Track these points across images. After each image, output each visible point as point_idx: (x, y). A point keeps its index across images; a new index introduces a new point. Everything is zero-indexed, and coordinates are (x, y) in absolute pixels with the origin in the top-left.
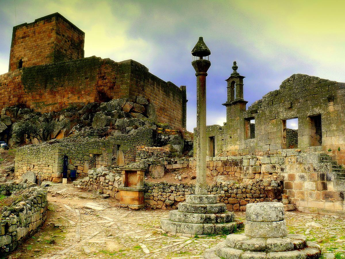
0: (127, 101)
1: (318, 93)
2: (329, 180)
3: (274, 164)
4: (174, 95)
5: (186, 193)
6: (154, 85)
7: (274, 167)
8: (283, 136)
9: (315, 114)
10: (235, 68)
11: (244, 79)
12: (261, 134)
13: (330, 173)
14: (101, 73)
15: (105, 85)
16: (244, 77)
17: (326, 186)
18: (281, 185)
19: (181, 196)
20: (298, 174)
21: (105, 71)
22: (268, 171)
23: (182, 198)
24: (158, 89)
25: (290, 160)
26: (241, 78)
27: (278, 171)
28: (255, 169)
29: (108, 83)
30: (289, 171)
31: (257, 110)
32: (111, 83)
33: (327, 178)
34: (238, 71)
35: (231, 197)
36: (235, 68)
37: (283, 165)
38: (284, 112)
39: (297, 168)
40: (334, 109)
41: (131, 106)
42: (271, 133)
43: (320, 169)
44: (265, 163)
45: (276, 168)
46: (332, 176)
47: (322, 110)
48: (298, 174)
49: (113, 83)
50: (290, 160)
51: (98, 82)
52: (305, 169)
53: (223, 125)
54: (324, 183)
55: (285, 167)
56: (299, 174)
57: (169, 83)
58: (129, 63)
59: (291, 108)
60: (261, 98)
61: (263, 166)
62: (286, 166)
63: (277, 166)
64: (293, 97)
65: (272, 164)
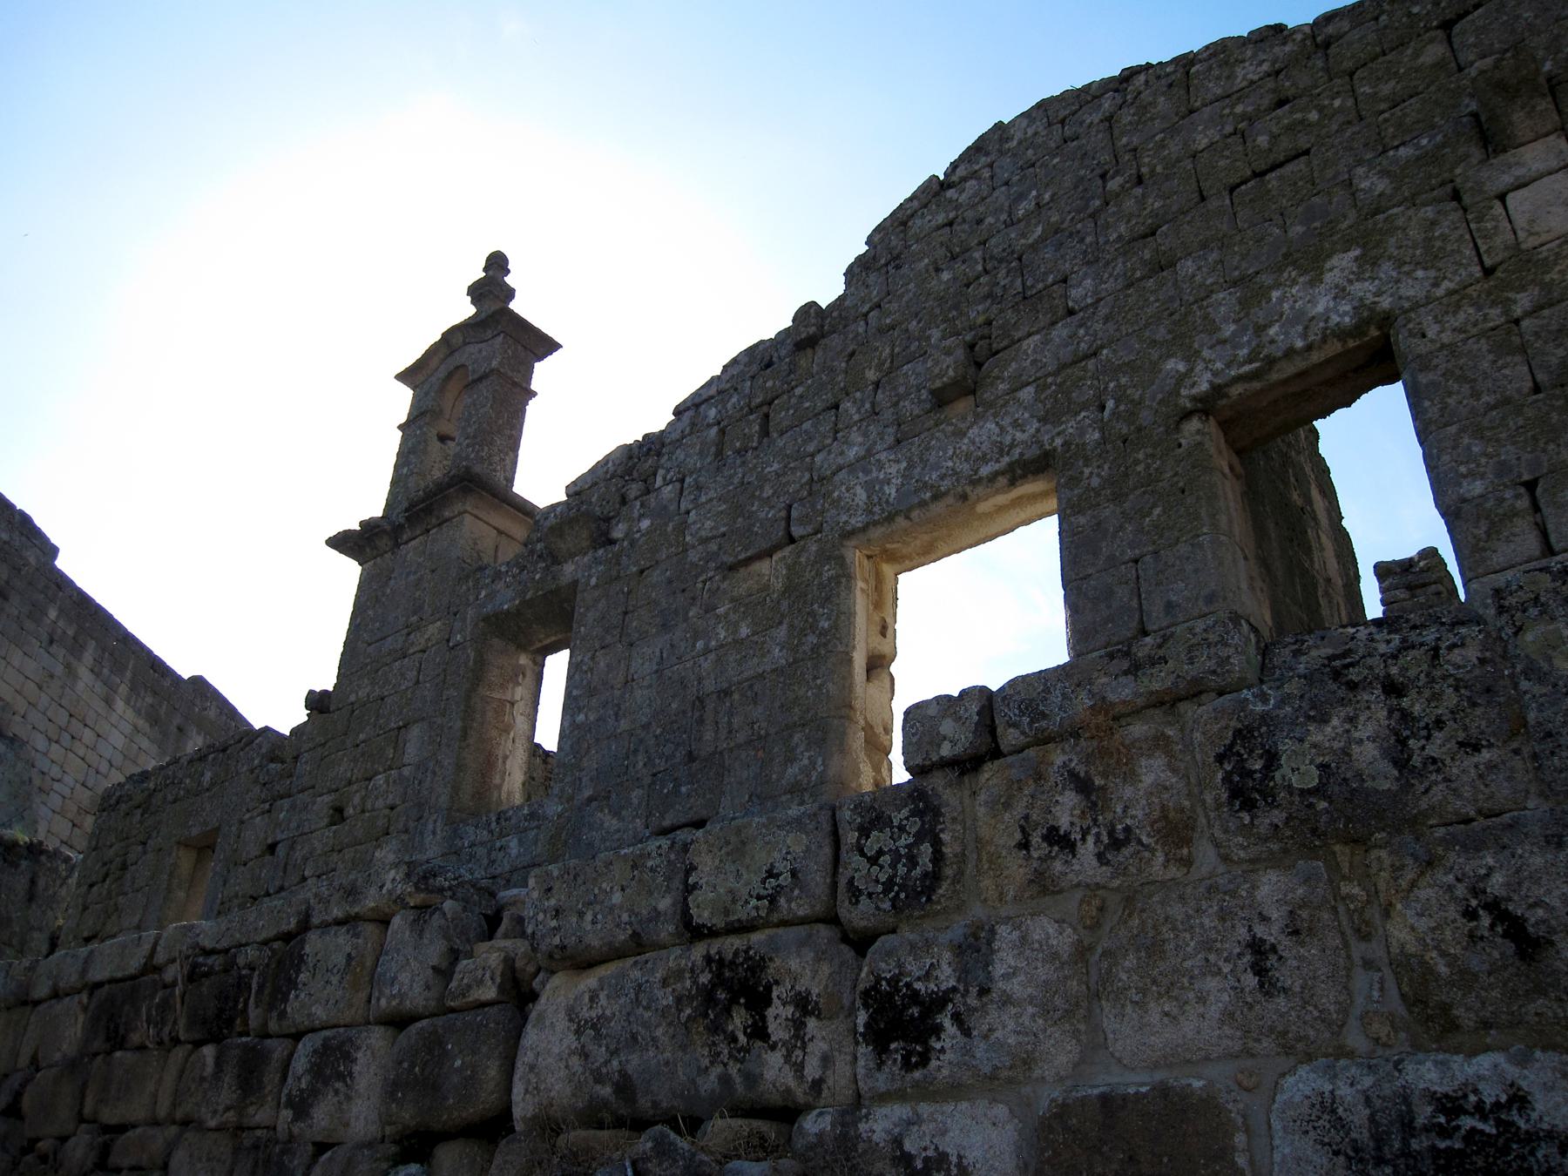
1: (1303, 142)
3: (731, 945)
7: (739, 989)
9: (1290, 353)
11: (544, 374)
12: (624, 725)
20: (1303, 1084)
22: (625, 1086)
24: (99, 688)
25: (1066, 810)
27: (812, 1070)
28: (416, 1079)
30: (1059, 1053)
31: (608, 520)
37: (907, 934)
38: (883, 456)
39: (1270, 933)
42: (726, 693)
44: (593, 932)
45: (778, 1015)
47: (1400, 263)
48: (1303, 1084)
50: (1066, 810)
52: (1514, 928)
53: (301, 716)
55: (963, 973)
56: (1350, 1088)
57: (199, 683)
59: (964, 390)
61: (559, 995)
62: (975, 949)
63: (802, 967)
64: (990, 295)
65: (698, 952)
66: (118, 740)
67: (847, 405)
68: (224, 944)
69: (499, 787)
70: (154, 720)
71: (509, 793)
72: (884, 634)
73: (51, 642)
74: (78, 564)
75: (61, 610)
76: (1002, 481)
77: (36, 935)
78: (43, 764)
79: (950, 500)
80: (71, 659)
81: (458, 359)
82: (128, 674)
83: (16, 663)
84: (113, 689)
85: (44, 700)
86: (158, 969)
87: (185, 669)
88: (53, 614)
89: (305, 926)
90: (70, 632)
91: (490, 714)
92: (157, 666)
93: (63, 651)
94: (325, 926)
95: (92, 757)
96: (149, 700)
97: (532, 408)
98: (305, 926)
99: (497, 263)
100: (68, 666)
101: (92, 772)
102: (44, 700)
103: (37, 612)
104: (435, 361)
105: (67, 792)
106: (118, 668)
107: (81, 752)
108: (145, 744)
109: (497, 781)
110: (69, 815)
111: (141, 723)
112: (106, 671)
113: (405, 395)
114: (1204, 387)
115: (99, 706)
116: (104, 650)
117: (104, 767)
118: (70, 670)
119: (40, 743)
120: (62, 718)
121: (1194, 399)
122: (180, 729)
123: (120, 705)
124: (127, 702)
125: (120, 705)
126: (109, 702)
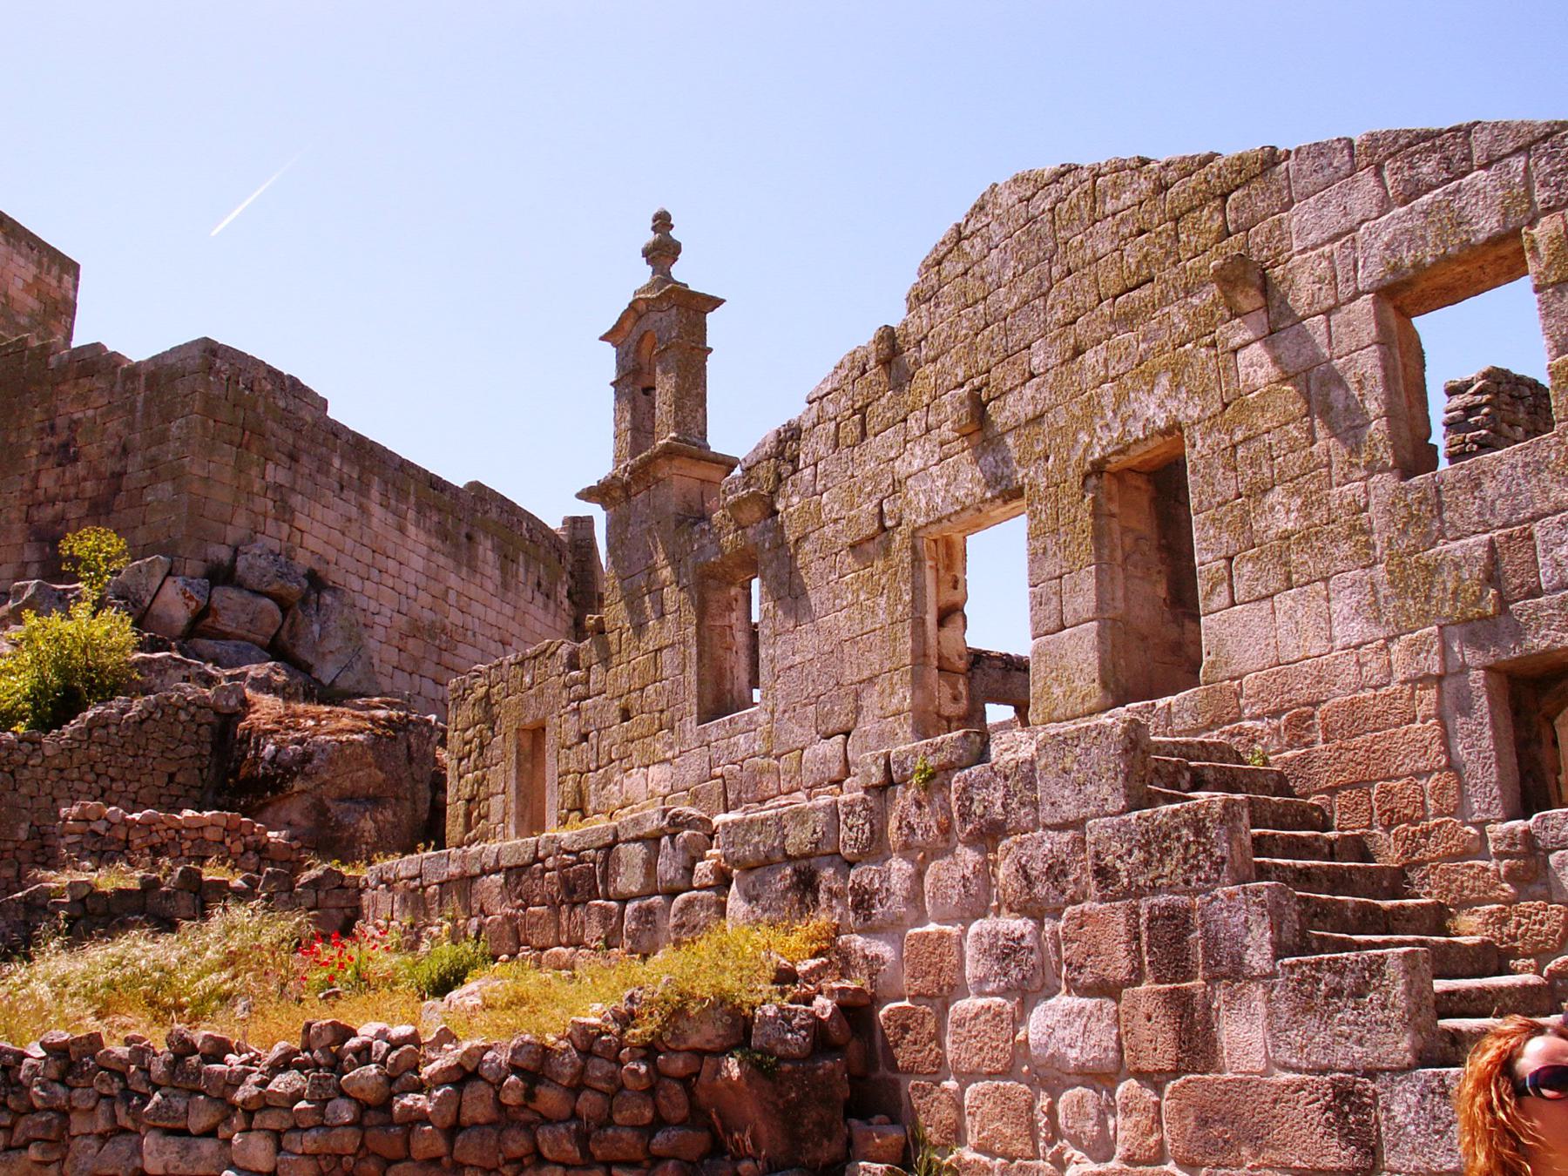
0: (169, 574)
2: (1234, 972)
4: (506, 560)
5: (78, 1124)
6: (364, 490)
8: (932, 651)
10: (663, 251)
11: (714, 321)
13: (1230, 896)
14: (53, 427)
15: (72, 491)
16: (716, 302)
17: (1208, 1025)
18: (853, 1044)
19: (34, 1153)
21: (76, 416)
23: (47, 1164)
24: (391, 519)
26: (698, 306)
29: (85, 479)
32: (99, 478)
33: (1211, 943)
34: (680, 272)
35: (408, 1158)
36: (663, 251)
40: (1276, 361)
41: (191, 598)
43: (1147, 863)
45: (823, 897)
46: (1245, 920)
49: (113, 474)
51: (35, 480)
54: (1188, 996)
57: (476, 487)
58: (193, 358)
60: (794, 409)
66: (417, 563)
67: (911, 422)
68: (576, 848)
69: (731, 691)
70: (444, 536)
71: (740, 692)
72: (955, 588)
73: (342, 488)
74: (349, 410)
75: (342, 457)
76: (999, 502)
77: (420, 786)
78: (362, 602)
79: (971, 511)
80: (364, 500)
81: (645, 325)
82: (412, 499)
83: (319, 517)
84: (402, 517)
85: (349, 544)
86: (542, 861)
87: (458, 478)
88: (337, 463)
89: (616, 841)
90: (355, 476)
91: (716, 638)
92: (436, 484)
93: (354, 494)
94: (627, 841)
95: (400, 585)
96: (435, 519)
97: (711, 362)
98: (616, 841)
99: (662, 222)
100: (361, 507)
101: (403, 598)
102: (349, 544)
103: (324, 466)
104: (628, 325)
105: (387, 622)
106: (402, 495)
107: (390, 582)
108: (442, 560)
109: (728, 687)
110: (394, 642)
111: (434, 541)
112: (393, 502)
113: (609, 352)
114: (1097, 455)
115: (395, 535)
116: (386, 483)
117: (412, 591)
118: (363, 509)
119: (355, 583)
120: (367, 556)
121: (1092, 463)
122: (469, 537)
123: (412, 530)
124: (417, 526)
125: (412, 530)
126: (402, 530)
